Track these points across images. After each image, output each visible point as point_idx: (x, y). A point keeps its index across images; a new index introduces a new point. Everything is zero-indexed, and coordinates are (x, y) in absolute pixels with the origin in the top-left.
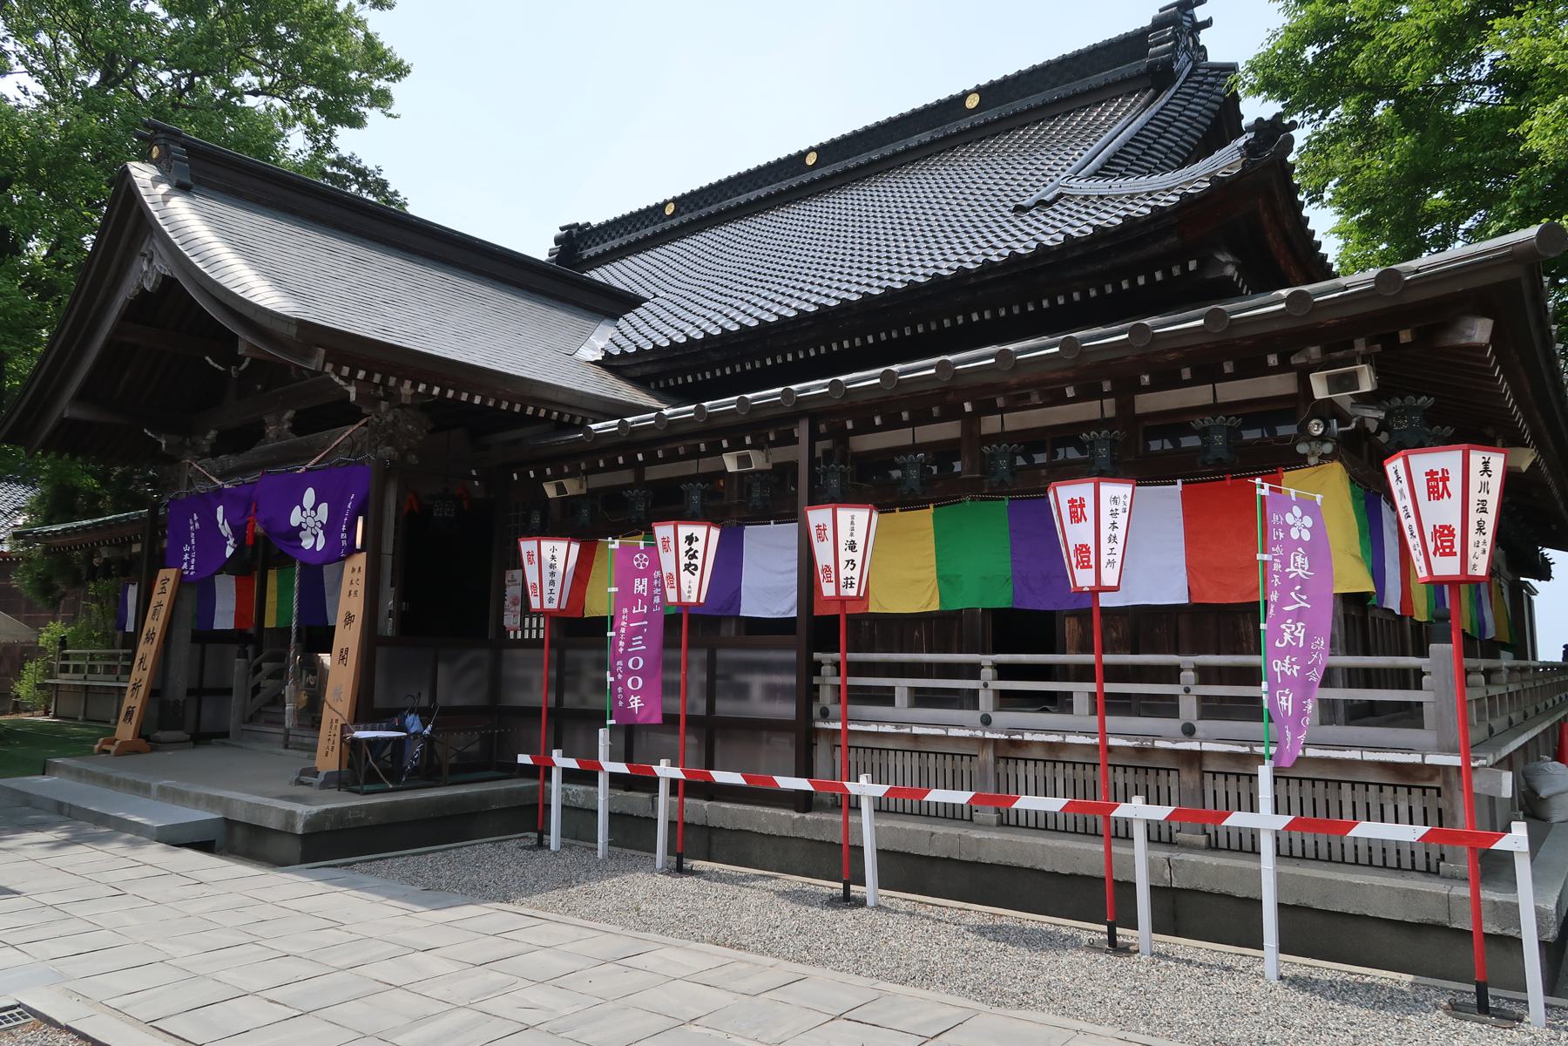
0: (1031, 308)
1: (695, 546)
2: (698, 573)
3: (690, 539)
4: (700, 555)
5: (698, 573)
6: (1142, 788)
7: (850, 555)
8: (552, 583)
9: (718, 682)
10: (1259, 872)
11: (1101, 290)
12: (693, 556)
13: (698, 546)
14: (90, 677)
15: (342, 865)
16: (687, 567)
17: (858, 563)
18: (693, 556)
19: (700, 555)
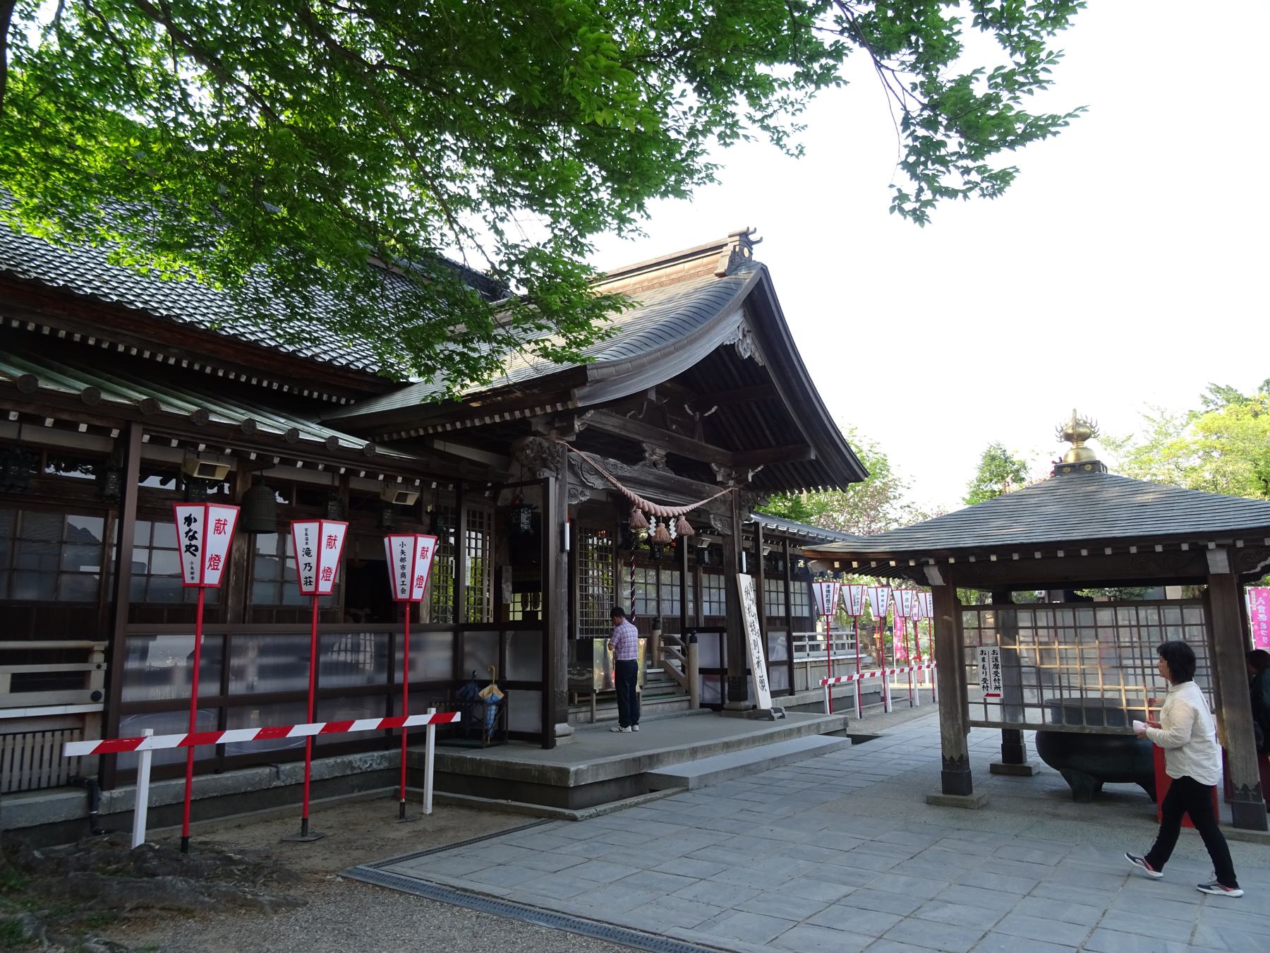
0: (221, 374)
1: (193, 526)
2: (199, 554)
3: (189, 520)
4: (199, 536)
5: (199, 554)
6: (64, 763)
7: (307, 559)
8: (403, 575)
9: (219, 658)
10: (434, 789)
11: (238, 376)
12: (193, 538)
13: (197, 527)
14: (812, 653)
15: (614, 810)
16: (188, 547)
17: (314, 565)
18: (193, 538)
19: (199, 536)
